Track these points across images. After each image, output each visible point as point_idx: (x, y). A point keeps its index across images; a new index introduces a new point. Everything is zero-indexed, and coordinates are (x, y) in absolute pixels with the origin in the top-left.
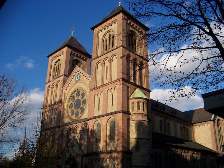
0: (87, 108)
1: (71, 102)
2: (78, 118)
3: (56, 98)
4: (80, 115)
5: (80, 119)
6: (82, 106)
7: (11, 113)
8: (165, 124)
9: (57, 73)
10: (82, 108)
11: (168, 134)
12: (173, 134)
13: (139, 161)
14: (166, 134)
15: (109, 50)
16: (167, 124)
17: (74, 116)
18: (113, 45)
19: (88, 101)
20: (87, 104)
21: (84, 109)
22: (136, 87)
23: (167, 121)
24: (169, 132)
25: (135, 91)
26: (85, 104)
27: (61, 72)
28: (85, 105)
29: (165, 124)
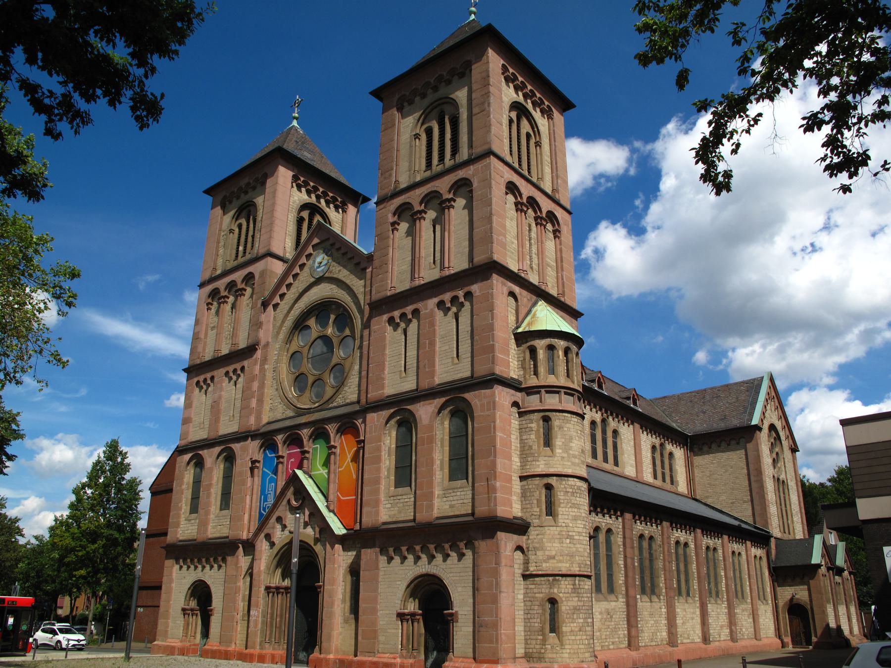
5: (335, 404)
13: (553, 553)
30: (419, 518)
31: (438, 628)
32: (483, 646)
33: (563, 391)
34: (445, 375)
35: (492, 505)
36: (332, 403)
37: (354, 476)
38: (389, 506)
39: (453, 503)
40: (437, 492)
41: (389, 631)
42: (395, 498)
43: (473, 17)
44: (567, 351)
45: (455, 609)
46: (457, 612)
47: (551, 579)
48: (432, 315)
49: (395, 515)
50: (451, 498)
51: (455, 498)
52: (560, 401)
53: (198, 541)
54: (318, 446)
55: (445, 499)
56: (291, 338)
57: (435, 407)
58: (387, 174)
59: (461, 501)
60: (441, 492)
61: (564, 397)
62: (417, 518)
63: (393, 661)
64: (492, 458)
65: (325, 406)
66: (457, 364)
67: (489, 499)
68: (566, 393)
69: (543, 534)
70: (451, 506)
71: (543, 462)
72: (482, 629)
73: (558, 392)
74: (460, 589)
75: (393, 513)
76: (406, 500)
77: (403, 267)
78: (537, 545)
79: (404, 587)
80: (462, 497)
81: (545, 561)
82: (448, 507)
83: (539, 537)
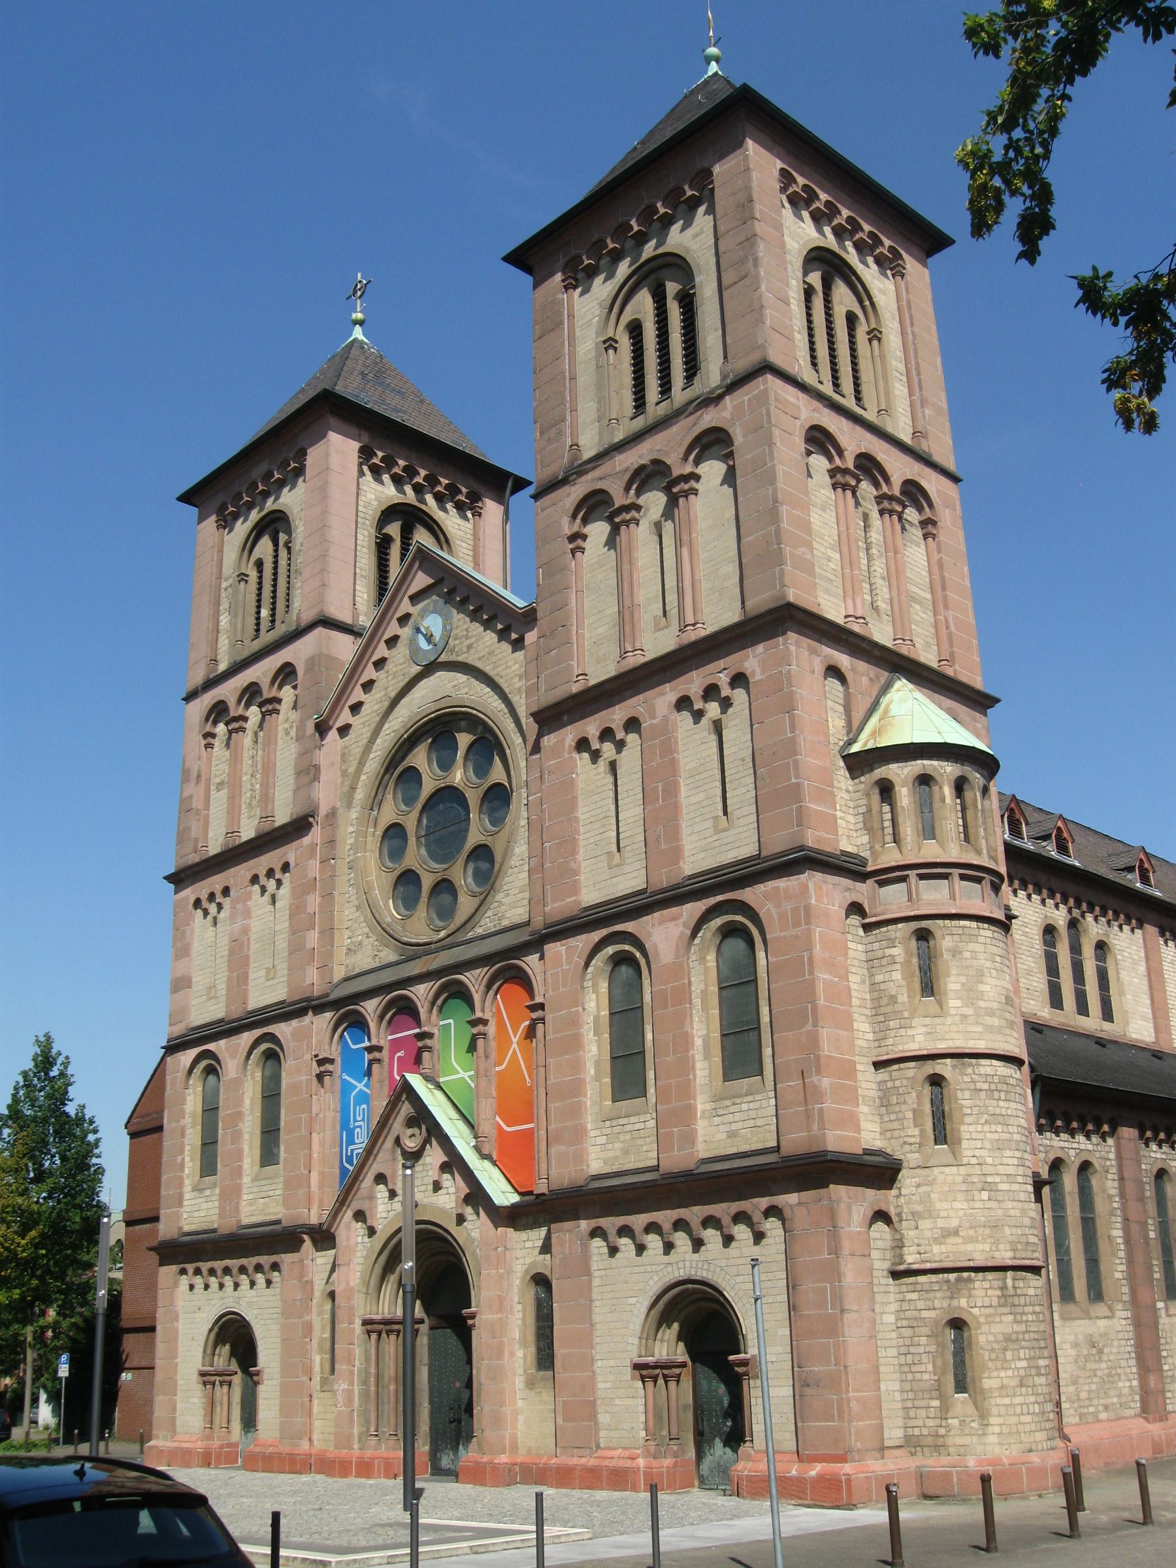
0: (521, 849)
1: (389, 813)
2: (452, 928)
3: (266, 798)
4: (466, 904)
5: (479, 931)
6: (474, 837)
7: (391, 1525)
8: (1076, 949)
9: (265, 613)
10: (483, 853)
11: (1107, 1026)
12: (217, 1211)
13: (954, 1223)
14: (1092, 1023)
15: (663, 409)
16: (1088, 952)
17: (421, 911)
18: (692, 367)
19: (520, 798)
20: (519, 814)
21: (498, 858)
22: (884, 675)
23: (1094, 928)
24: (1108, 1015)
25: (885, 701)
26: (498, 821)
27: (297, 603)
28: (503, 835)
29: (1076, 949)
34: (702, 855)
38: (603, 1140)
39: (734, 1127)
40: (702, 1104)
41: (618, 1402)
42: (614, 1123)
45: (752, 1351)
47: (952, 1277)
48: (665, 729)
49: (616, 1157)
50: (730, 1118)
51: (738, 1116)
54: (451, 1021)
55: (717, 1120)
56: (379, 797)
57: (685, 925)
59: (751, 1123)
60: (708, 1106)
64: (809, 1027)
65: (460, 937)
66: (724, 830)
67: (808, 1115)
69: (930, 1183)
70: (732, 1135)
75: (611, 1154)
76: (637, 1126)
78: (919, 1208)
80: (753, 1114)
81: (937, 1241)
82: (724, 1136)
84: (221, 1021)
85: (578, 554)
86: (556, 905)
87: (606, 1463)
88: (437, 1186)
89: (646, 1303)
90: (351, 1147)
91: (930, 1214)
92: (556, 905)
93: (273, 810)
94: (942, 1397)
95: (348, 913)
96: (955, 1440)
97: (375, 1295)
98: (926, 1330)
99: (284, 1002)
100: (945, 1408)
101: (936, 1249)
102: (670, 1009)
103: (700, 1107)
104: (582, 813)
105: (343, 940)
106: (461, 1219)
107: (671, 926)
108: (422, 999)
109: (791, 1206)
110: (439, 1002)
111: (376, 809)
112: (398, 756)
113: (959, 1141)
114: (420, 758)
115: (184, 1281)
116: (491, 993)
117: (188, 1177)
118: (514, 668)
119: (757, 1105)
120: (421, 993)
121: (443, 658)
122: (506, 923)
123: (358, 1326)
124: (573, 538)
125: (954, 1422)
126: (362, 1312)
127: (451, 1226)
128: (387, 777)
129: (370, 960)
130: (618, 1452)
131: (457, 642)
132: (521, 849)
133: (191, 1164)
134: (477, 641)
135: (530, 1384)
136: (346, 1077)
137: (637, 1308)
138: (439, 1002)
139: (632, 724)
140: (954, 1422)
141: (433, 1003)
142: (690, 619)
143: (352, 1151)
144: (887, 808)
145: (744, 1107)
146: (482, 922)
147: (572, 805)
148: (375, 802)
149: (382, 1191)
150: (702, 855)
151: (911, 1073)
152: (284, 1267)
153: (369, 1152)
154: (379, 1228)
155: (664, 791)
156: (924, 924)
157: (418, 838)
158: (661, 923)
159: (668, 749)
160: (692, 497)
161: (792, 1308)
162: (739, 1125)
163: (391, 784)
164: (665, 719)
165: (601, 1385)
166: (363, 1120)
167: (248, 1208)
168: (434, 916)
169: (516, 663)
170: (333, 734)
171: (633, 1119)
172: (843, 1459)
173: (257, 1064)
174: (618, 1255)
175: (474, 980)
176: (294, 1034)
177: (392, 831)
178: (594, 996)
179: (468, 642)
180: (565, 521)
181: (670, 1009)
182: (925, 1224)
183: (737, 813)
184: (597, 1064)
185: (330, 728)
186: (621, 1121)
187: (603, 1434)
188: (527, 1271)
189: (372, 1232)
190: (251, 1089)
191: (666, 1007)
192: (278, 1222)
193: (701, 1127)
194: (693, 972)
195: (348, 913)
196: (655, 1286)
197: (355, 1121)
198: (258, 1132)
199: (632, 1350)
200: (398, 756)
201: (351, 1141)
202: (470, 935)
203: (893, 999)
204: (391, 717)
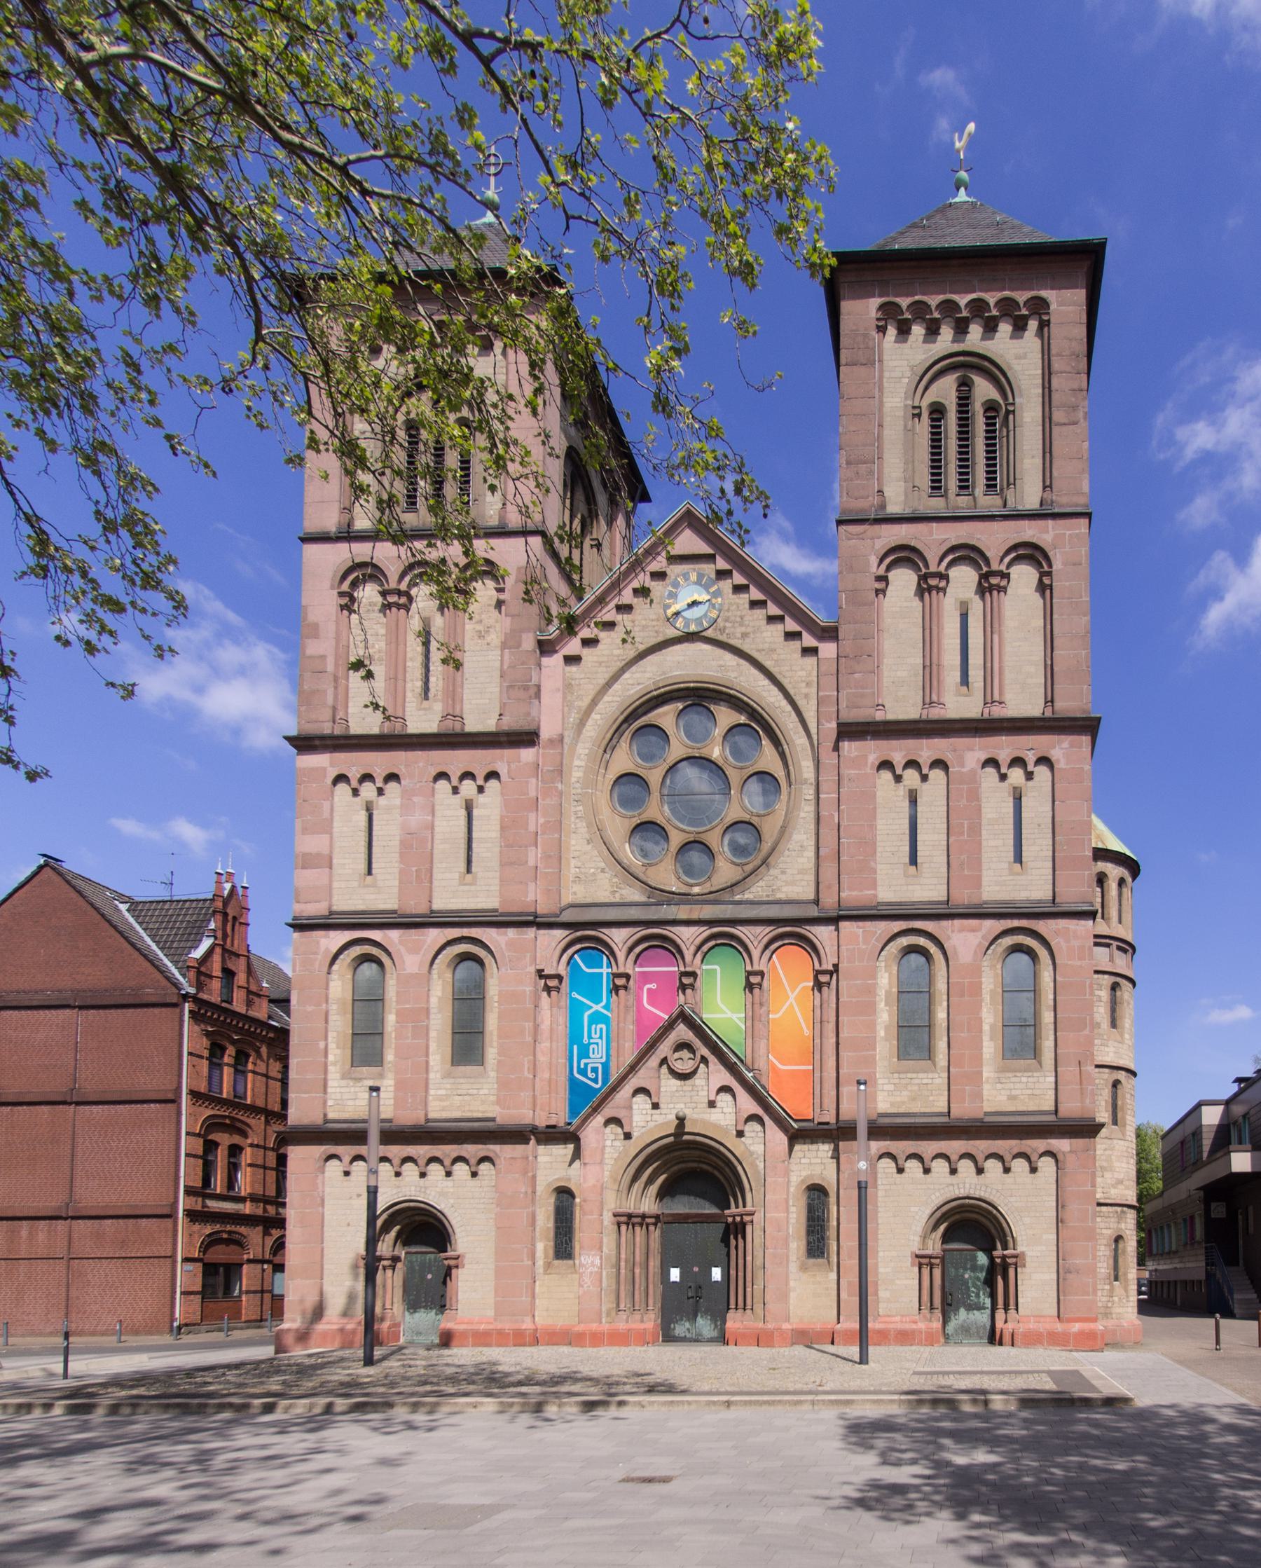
5: (748, 896)
13: (1122, 1176)
30: (955, 1113)
31: (967, 1276)
32: (1071, 1299)
33: (1115, 943)
34: (997, 888)
35: (1088, 1101)
36: (742, 892)
37: (807, 1032)
38: (891, 1087)
39: (1014, 1093)
40: (988, 1072)
41: (898, 1282)
42: (902, 1076)
43: (962, 196)
44: (1121, 882)
45: (1020, 1249)
46: (1023, 1253)
47: (1119, 1209)
48: (972, 779)
49: (903, 1103)
50: (1012, 1086)
51: (1018, 1086)
52: (1111, 960)
53: (396, 1123)
54: (717, 967)
55: (999, 1086)
56: (614, 741)
57: (984, 937)
58: (863, 468)
59: (1029, 1092)
60: (992, 1075)
61: (1117, 953)
62: (1061, 1108)
63: (914, 1326)
64: (1087, 1032)
65: (726, 896)
66: (1018, 874)
67: (1082, 1092)
68: (1119, 948)
69: (1112, 1149)
70: (1012, 1098)
71: (1112, 1049)
72: (1069, 1276)
73: (1108, 945)
74: (1027, 1220)
75: (899, 1099)
76: (925, 1081)
77: (899, 674)
78: (1105, 1164)
79: (926, 1216)
80: (1030, 1085)
81: (1114, 1186)
82: (1005, 1098)
83: (1108, 1152)
84: (395, 912)
85: (881, 596)
86: (854, 893)
87: (891, 1326)
88: (712, 1104)
89: (928, 1211)
90: (583, 1061)
91: (1111, 1169)
92: (854, 893)
93: (462, 710)
94: (1111, 1284)
95: (578, 842)
96: (1116, 1310)
97: (625, 1192)
98: (1104, 1242)
99: (496, 910)
100: (1112, 1290)
101: (1113, 1191)
102: (966, 998)
103: (985, 1075)
104: (881, 824)
105: (571, 869)
106: (740, 1134)
107: (970, 936)
108: (688, 944)
109: (1064, 1153)
110: (705, 948)
111: (609, 752)
112: (640, 711)
113: (1125, 1125)
114: (666, 716)
115: (334, 1167)
116: (768, 953)
117: (334, 1064)
118: (800, 673)
119: (1035, 1080)
120: (688, 936)
121: (709, 633)
122: (781, 896)
123: (608, 1218)
124: (879, 579)
125: (1116, 1299)
126: (613, 1206)
127: (731, 1142)
128: (625, 726)
129: (607, 893)
130: (898, 1319)
131: (728, 625)
132: (802, 836)
133: (337, 1053)
134: (754, 632)
135: (803, 1268)
136: (575, 995)
137: (921, 1214)
138: (705, 948)
139: (939, 764)
140: (1116, 1299)
141: (631, 949)
142: (996, 697)
143: (586, 1065)
144: (1099, 890)
145: (1024, 1079)
146: (753, 889)
147: (873, 815)
148: (610, 746)
149: (641, 1102)
150: (997, 888)
151: (1106, 1076)
152: (501, 1162)
153: (633, 1068)
154: (635, 1134)
155: (969, 828)
156: (1119, 979)
157: (662, 795)
158: (961, 930)
159: (974, 795)
160: (1002, 594)
161: (1059, 1220)
162: (1018, 1092)
163: (628, 735)
164: (973, 771)
165: (881, 1270)
166: (601, 1037)
167: (437, 1103)
168: (680, 871)
169: (802, 669)
170: (557, 659)
171: (921, 1075)
172: (1095, 1320)
173: (449, 965)
174: (904, 1175)
175: (754, 936)
176: (511, 944)
177: (625, 779)
178: (886, 975)
179: (743, 629)
180: (874, 560)
181: (966, 998)
182: (1108, 1175)
183: (1030, 865)
184: (887, 1028)
185: (556, 652)
186: (909, 1075)
187: (881, 1305)
188: (803, 1181)
189: (628, 1136)
190: (440, 988)
191: (963, 996)
192: (493, 1120)
193: (987, 1090)
194: (984, 974)
195: (578, 842)
196: (937, 1198)
197: (590, 1037)
198: (450, 1031)
199: (915, 1245)
200: (640, 711)
201: (584, 1053)
202: (738, 898)
203: (1098, 1025)
204: (634, 668)
